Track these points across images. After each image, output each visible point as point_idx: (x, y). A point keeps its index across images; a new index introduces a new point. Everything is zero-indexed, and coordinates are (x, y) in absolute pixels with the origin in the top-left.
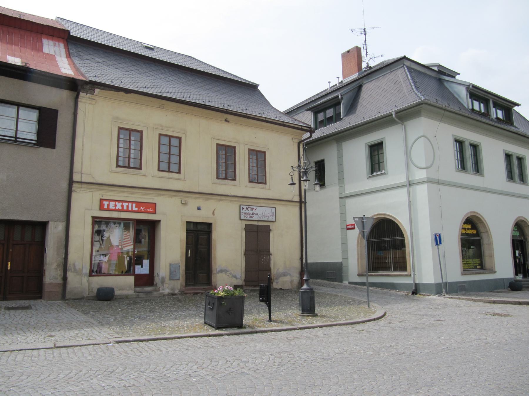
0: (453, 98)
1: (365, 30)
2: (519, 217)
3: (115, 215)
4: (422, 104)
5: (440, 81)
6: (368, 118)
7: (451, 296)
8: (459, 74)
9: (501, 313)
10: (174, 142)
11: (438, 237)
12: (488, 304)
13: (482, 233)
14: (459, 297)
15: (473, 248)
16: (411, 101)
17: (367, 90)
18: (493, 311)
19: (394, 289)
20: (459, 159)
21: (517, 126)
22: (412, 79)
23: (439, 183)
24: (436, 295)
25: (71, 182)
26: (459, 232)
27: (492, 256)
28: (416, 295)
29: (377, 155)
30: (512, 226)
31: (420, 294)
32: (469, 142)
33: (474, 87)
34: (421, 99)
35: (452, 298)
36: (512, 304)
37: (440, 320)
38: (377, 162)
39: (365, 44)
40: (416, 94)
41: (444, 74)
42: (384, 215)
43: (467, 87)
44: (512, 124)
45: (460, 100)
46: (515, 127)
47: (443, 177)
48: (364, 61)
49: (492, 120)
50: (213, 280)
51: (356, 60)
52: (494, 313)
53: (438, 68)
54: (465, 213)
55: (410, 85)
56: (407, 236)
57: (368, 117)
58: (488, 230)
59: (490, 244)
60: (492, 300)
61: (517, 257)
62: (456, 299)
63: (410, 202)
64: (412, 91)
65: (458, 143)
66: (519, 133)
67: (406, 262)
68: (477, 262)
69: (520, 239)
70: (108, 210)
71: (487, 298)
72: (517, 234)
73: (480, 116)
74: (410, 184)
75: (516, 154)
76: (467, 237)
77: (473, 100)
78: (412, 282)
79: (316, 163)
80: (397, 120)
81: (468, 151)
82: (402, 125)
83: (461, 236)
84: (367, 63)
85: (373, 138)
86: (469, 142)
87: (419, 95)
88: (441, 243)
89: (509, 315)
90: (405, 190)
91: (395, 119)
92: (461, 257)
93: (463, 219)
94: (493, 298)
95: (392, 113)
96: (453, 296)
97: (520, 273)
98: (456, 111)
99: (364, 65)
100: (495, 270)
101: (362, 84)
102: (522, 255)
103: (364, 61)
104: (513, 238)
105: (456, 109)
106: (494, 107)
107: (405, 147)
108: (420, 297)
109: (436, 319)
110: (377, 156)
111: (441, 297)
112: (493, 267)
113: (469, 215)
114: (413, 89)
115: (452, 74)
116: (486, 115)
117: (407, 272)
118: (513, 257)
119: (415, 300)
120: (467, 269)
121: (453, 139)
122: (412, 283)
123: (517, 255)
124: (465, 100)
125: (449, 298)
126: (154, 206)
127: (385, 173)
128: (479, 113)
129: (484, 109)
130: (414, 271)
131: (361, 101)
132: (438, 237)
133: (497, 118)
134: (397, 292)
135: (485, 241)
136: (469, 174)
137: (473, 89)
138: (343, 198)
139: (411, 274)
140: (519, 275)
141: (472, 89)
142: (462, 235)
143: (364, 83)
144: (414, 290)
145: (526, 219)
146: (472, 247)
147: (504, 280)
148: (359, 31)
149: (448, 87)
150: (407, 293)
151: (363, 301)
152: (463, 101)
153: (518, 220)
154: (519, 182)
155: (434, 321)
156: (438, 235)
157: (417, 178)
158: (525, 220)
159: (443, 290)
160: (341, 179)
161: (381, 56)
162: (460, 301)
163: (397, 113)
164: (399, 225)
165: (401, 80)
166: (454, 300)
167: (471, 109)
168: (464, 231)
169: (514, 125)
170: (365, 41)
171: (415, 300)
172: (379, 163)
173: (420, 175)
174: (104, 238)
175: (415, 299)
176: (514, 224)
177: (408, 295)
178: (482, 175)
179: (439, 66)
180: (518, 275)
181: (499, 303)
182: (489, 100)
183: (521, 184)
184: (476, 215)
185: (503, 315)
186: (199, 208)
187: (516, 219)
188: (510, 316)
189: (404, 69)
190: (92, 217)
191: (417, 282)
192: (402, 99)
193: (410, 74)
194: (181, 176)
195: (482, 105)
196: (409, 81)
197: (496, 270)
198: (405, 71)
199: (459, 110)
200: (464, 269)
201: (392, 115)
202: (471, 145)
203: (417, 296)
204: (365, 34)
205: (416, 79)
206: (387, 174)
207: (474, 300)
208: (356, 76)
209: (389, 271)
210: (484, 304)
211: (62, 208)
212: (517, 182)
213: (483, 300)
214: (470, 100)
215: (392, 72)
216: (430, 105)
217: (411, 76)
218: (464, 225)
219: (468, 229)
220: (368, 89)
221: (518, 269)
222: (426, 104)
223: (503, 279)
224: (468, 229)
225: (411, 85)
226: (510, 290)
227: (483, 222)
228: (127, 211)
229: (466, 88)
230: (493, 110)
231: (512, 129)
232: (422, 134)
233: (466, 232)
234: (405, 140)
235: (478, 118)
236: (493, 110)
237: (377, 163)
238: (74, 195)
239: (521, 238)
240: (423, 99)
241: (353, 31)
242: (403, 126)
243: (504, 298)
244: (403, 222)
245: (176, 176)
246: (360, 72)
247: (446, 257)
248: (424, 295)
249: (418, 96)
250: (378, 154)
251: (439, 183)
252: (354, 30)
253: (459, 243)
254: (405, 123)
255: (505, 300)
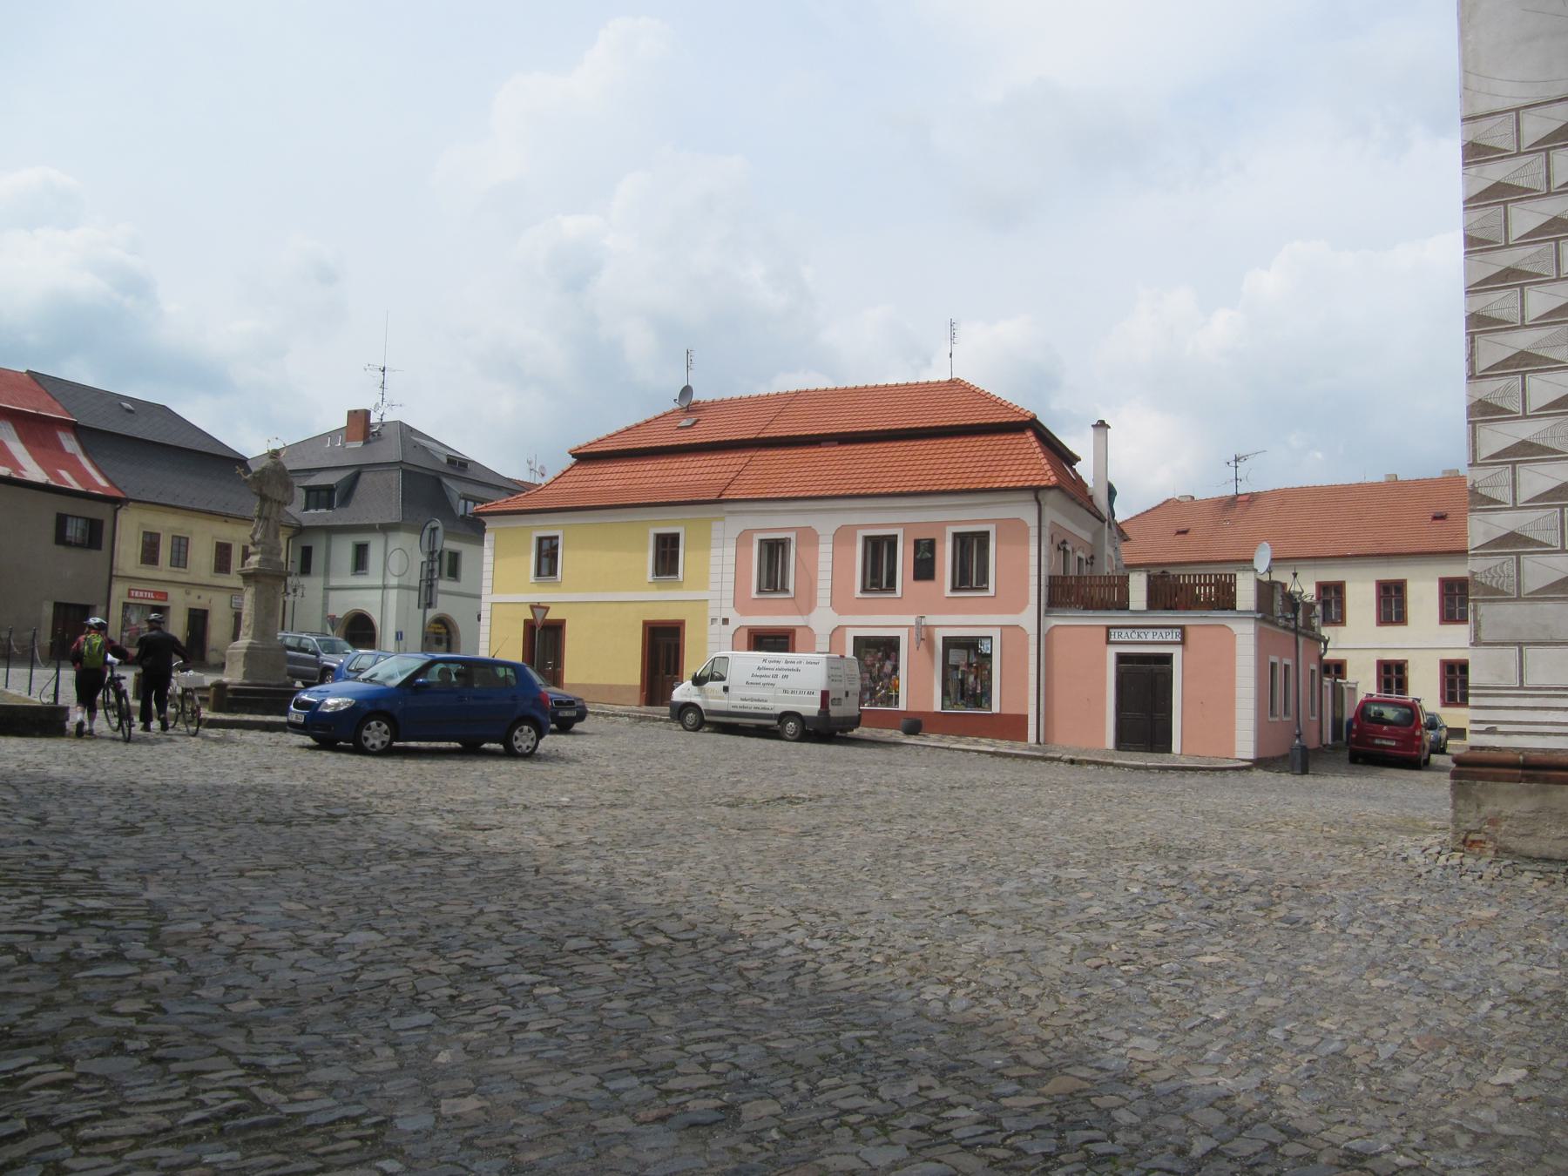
3: (138, 601)
10: (183, 542)
13: (8, 668)
25: (111, 576)
50: (207, 656)
54: (445, 612)
70: (134, 597)
74: (384, 587)
79: (303, 548)
85: (361, 538)
90: (381, 591)
126: (166, 594)
131: (356, 492)
138: (328, 589)
151: (360, 749)
160: (327, 572)
173: (393, 581)
186: (199, 597)
194: (187, 571)
211: (105, 595)
228: (147, 598)
238: (113, 586)
244: (376, 618)
245: (183, 570)
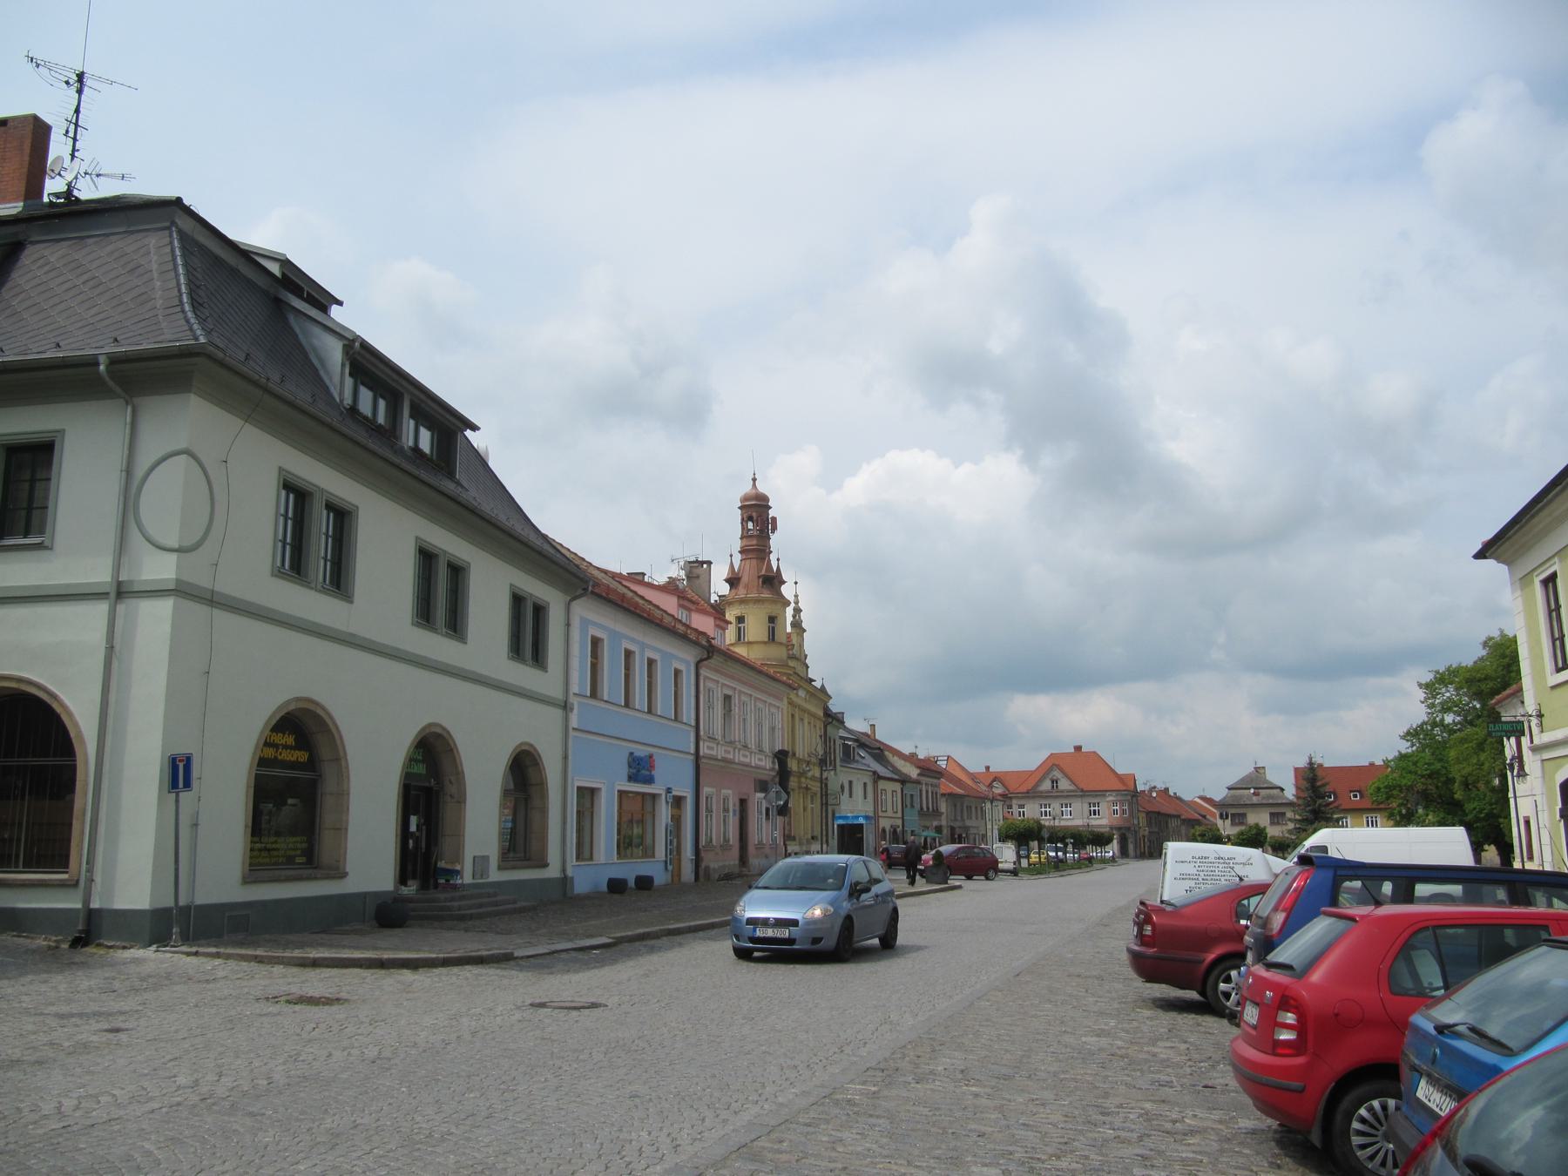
0: (304, 365)
1: (81, 77)
2: (430, 725)
4: (198, 354)
5: (279, 307)
6: (14, 354)
7: (194, 949)
8: (340, 303)
9: (318, 996)
11: (181, 766)
12: (295, 970)
13: (324, 761)
14: (219, 950)
15: (294, 805)
16: (169, 337)
17: (39, 264)
18: (296, 990)
19: (13, 931)
20: (289, 540)
21: (465, 484)
22: (188, 273)
23: (212, 601)
24: (150, 946)
26: (254, 753)
27: (341, 829)
28: (84, 949)
29: (25, 481)
30: (410, 748)
31: (99, 945)
32: (324, 498)
33: (365, 346)
34: (196, 339)
35: (196, 954)
36: (361, 966)
37: (117, 1030)
38: (25, 505)
39: (74, 121)
40: (188, 321)
41: (297, 291)
42: (20, 680)
43: (346, 342)
44: (451, 474)
45: (322, 373)
46: (458, 483)
47: (227, 585)
48: (59, 174)
49: (400, 451)
51: (27, 158)
52: (301, 997)
53: (281, 266)
55: (176, 289)
56: (86, 754)
57: (16, 351)
58: (341, 754)
59: (343, 795)
60: (309, 958)
61: (413, 833)
62: (209, 959)
63: (110, 649)
64: (179, 309)
65: (291, 496)
66: (460, 499)
67: (69, 841)
68: (299, 845)
69: (427, 784)
71: (297, 953)
72: (420, 769)
73: (367, 432)
74: (121, 592)
75: (447, 555)
76: (277, 772)
77: (359, 382)
78: (79, 906)
80: (111, 383)
81: (321, 523)
82: (127, 403)
83: (258, 766)
84: (71, 182)
86: (324, 498)
87: (196, 327)
88: (187, 784)
89: (338, 1000)
90: (103, 607)
91: (107, 379)
92: (250, 830)
93: (270, 718)
94: (314, 952)
95: (97, 359)
96: (201, 950)
97: (414, 878)
98: (298, 401)
99: (53, 186)
100: (345, 868)
101: (25, 240)
102: (424, 827)
103: (59, 174)
104: (407, 782)
105: (302, 397)
106: (412, 416)
107: (124, 473)
108: (95, 954)
109: (106, 1026)
110: (26, 486)
111: (164, 952)
112: (338, 861)
113: (292, 707)
114: (181, 303)
115: (322, 300)
116: (390, 433)
117: (67, 872)
118: (399, 832)
119: (77, 963)
120: (260, 864)
121: (279, 479)
122: (78, 910)
123: (413, 828)
124: (337, 379)
125: (188, 954)
127: (46, 544)
128: (369, 424)
129: (386, 417)
130: (90, 870)
132: (181, 766)
133: (416, 449)
134: (22, 939)
135: (329, 785)
136: (312, 588)
137: (363, 352)
139: (78, 881)
140: (410, 882)
141: (359, 353)
142: (263, 762)
143: (32, 239)
144: (80, 932)
145: (448, 732)
146: (290, 801)
147: (365, 898)
148: (59, 71)
149: (297, 330)
150: (55, 941)
152: (331, 379)
153: (427, 731)
154: (444, 630)
155: (95, 1033)
156: (180, 761)
157: (144, 578)
158: (445, 735)
159: (174, 930)
161: (123, 177)
162: (217, 962)
163: (115, 361)
164: (64, 717)
165: (155, 266)
166: (203, 959)
167: (348, 407)
168: (270, 753)
169: (455, 477)
170: (77, 111)
171: (77, 963)
172: (30, 509)
173: (159, 568)
174: (1501, 707)
175: (76, 960)
176: (415, 743)
177: (57, 947)
178: (349, 597)
179: (286, 263)
180: (406, 885)
181: (328, 966)
182: (402, 394)
183: (447, 635)
184: (312, 707)
185: (323, 1000)
187: (423, 729)
188: (341, 1002)
189: (171, 236)
190: (352, 602)
191: (95, 904)
192: (142, 324)
193: (183, 256)
195: (382, 404)
196: (177, 276)
197: (347, 870)
198: (171, 243)
199: (310, 400)
200: (251, 865)
201: (97, 364)
202: (330, 507)
203: (90, 950)
204: (80, 92)
205: (200, 277)
206: (51, 549)
207: (259, 960)
208: (14, 212)
209: (10, 867)
210: (284, 970)
212: (439, 631)
213: (285, 957)
214: (349, 382)
215: (132, 232)
216: (223, 364)
217: (185, 265)
218: (274, 734)
219: (286, 747)
220: (41, 261)
221: (410, 868)
222: (210, 357)
223: (363, 896)
224: (286, 747)
225: (179, 290)
226: (377, 925)
227: (329, 731)
229: (344, 345)
230: (409, 425)
231: (448, 486)
232: (183, 445)
233: (276, 758)
234: (126, 452)
235: (361, 435)
236: (409, 425)
237: (24, 509)
239: (430, 782)
240: (202, 340)
241: (38, 65)
242: (129, 409)
243: (347, 951)
246: (30, 202)
247: (199, 827)
248: (111, 947)
249: (191, 329)
250: (33, 481)
251: (212, 601)
252: (43, 63)
253: (248, 787)
254: (137, 400)
255: (345, 956)
